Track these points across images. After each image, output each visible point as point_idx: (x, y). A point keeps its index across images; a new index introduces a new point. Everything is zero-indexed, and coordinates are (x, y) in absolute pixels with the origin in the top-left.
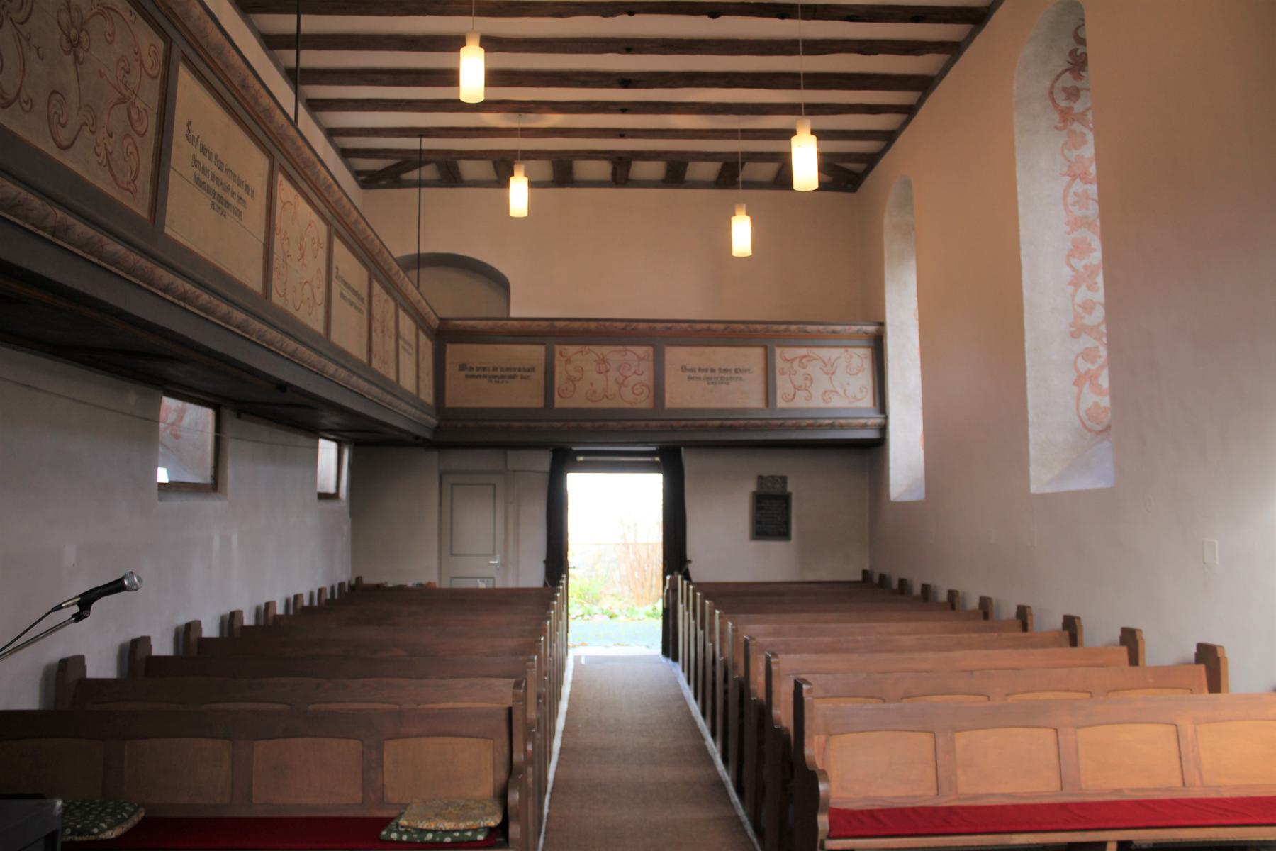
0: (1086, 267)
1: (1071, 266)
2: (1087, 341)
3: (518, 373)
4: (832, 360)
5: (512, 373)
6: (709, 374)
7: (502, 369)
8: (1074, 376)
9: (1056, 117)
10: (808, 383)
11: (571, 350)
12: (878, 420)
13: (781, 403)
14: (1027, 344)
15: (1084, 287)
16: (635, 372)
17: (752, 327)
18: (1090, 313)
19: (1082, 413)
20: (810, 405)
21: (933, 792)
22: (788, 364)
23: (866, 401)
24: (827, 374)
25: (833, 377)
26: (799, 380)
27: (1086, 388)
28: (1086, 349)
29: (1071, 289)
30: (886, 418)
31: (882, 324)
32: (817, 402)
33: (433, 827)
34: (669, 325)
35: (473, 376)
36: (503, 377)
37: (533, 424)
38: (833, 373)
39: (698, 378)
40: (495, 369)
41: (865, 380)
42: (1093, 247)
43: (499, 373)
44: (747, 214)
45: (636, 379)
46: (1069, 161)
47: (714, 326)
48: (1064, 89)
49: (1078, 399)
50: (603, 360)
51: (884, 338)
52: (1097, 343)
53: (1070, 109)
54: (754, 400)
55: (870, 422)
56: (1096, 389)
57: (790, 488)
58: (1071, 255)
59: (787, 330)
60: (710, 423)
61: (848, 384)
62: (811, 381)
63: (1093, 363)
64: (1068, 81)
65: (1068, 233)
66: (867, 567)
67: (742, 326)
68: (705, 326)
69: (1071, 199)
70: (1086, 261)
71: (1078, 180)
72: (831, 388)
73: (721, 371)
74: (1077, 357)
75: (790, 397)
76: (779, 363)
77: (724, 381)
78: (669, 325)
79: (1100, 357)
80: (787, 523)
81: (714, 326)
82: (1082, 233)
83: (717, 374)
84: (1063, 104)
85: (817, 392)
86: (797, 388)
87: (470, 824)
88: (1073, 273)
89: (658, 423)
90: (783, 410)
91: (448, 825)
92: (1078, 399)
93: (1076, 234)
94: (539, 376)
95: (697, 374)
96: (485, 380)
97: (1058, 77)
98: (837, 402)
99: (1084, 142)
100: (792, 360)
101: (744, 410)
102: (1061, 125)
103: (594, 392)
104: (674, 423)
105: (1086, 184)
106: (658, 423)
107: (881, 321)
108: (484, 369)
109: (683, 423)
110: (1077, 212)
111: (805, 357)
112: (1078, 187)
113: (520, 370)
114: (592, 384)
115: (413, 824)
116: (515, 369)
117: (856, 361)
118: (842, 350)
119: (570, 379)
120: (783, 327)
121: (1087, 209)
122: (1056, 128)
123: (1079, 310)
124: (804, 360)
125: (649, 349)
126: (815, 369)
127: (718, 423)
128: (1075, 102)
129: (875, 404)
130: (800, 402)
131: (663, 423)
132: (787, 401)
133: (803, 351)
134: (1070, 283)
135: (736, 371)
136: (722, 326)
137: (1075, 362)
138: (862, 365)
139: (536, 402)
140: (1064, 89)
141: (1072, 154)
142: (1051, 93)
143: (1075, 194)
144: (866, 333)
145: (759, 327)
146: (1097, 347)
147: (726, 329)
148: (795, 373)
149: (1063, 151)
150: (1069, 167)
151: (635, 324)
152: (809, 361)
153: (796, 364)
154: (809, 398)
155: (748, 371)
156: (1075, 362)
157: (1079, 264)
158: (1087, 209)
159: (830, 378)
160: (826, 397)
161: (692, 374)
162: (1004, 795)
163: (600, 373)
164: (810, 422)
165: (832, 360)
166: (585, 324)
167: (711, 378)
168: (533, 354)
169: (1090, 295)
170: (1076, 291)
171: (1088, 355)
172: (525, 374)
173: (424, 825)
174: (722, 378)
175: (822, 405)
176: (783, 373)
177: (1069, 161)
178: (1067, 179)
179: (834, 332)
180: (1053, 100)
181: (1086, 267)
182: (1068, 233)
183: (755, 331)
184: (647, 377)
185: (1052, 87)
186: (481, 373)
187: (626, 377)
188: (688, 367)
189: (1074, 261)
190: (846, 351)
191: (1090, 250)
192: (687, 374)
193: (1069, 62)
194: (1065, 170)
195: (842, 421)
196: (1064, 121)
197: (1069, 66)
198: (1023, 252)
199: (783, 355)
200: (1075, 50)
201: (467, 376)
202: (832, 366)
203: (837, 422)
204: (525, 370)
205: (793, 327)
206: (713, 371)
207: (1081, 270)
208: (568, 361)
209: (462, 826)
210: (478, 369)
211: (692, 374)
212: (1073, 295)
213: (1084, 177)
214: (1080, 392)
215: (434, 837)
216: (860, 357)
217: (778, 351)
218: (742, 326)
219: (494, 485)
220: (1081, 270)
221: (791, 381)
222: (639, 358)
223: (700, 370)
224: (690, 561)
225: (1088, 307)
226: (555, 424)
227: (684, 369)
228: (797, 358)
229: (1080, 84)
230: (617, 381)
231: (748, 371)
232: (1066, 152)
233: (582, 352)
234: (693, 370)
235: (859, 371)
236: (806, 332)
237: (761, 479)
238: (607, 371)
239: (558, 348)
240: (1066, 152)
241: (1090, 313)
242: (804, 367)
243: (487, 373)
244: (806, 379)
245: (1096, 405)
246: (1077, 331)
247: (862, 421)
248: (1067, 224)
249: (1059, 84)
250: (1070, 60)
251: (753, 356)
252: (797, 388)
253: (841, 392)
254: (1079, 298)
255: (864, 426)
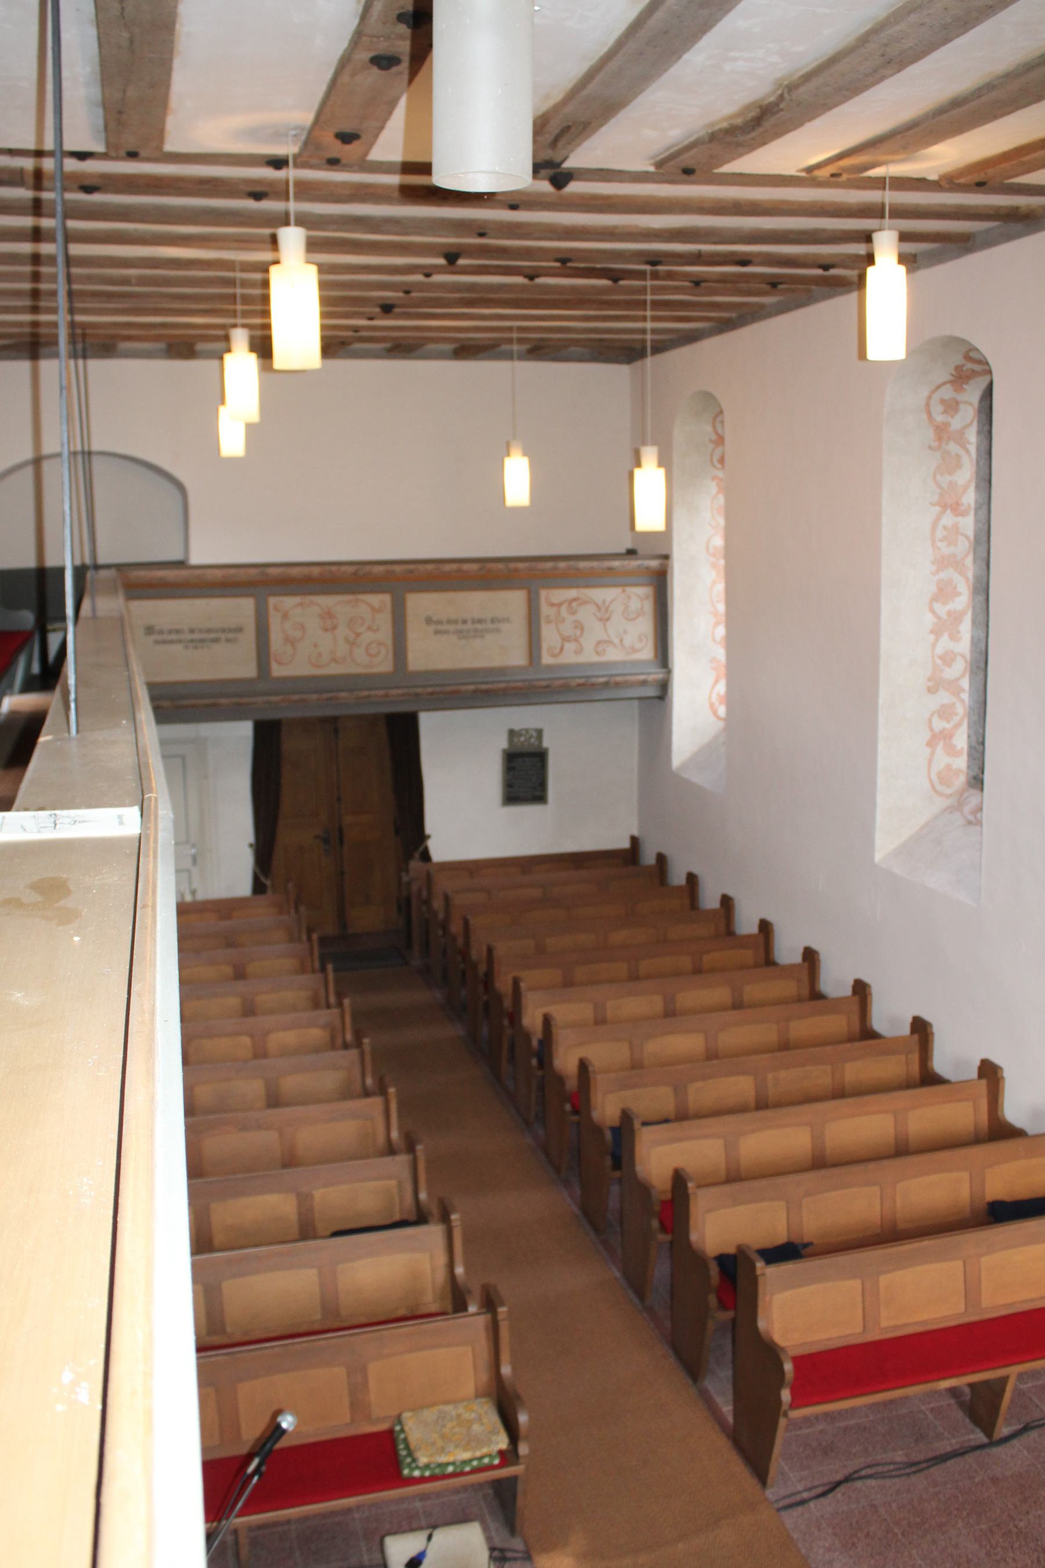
0: (949, 613)
1: (932, 611)
2: (944, 697)
3: (223, 636)
4: (607, 603)
5: (213, 636)
6: (460, 627)
7: (201, 631)
8: (928, 735)
9: (931, 433)
10: (578, 632)
11: (289, 602)
12: (658, 675)
13: (547, 659)
14: (881, 701)
15: (945, 637)
16: (369, 628)
17: (512, 565)
18: (950, 665)
19: (934, 777)
20: (581, 659)
21: (860, 1329)
22: (554, 610)
23: (647, 652)
24: (600, 620)
25: (608, 624)
26: (568, 629)
27: (940, 748)
28: (943, 706)
29: (932, 637)
30: (669, 672)
31: (666, 557)
32: (589, 656)
33: (451, 1459)
34: (411, 567)
35: (164, 642)
36: (203, 641)
37: (244, 700)
38: (608, 619)
39: (447, 632)
40: (192, 631)
41: (645, 625)
42: (945, 543)
43: (197, 636)
44: (525, 454)
45: (368, 637)
46: (941, 488)
47: (466, 567)
48: (943, 401)
49: (930, 761)
50: (328, 615)
51: (669, 577)
52: (954, 700)
53: (946, 425)
54: (517, 658)
55: (651, 678)
56: (952, 751)
57: (546, 743)
58: (935, 599)
59: (555, 568)
60: (464, 688)
61: (625, 632)
62: (582, 629)
63: (948, 721)
64: (948, 393)
65: (933, 574)
66: (636, 833)
67: (501, 566)
68: (454, 566)
69: (940, 533)
70: (950, 606)
71: (949, 511)
72: (605, 638)
73: (474, 621)
74: (932, 715)
75: (557, 651)
76: (545, 610)
77: (478, 634)
78: (411, 567)
79: (956, 714)
80: (542, 785)
81: (466, 567)
82: (950, 573)
83: (469, 626)
84: (940, 418)
85: (589, 642)
86: (565, 639)
87: (485, 1450)
88: (935, 620)
89: (400, 691)
90: (550, 667)
91: (466, 1455)
92: (930, 761)
93: (942, 575)
94: (249, 637)
95: (446, 627)
96: (179, 647)
97: (938, 387)
98: (613, 655)
99: (959, 466)
100: (559, 605)
101: (502, 671)
102: (935, 444)
103: (320, 655)
104: (419, 690)
105: (957, 515)
106: (400, 691)
107: (664, 552)
108: (178, 632)
109: (430, 690)
110: (946, 550)
111: (575, 600)
112: (948, 519)
113: (223, 630)
114: (315, 645)
115: (433, 1460)
116: (217, 631)
117: (635, 604)
118: (619, 590)
119: (289, 640)
120: (549, 565)
121: (956, 546)
122: (930, 447)
123: (939, 662)
124: (574, 605)
125: (387, 598)
126: (585, 614)
127: (472, 687)
128: (952, 417)
129: (656, 656)
130: (569, 657)
131: (405, 690)
132: (554, 656)
133: (573, 593)
134: (932, 632)
135: (493, 621)
136: (475, 567)
137: (930, 721)
138: (642, 607)
139: (248, 670)
140: (943, 401)
141: (945, 480)
142: (928, 405)
143: (945, 528)
144: (648, 568)
145: (521, 565)
146: (954, 704)
147: (481, 569)
148: (563, 621)
149: (935, 476)
150: (941, 495)
151: (368, 568)
152: (580, 605)
153: (564, 609)
154: (579, 651)
155: (507, 620)
156: (930, 721)
157: (942, 610)
158: (956, 546)
159: (605, 626)
160: (600, 649)
161: (440, 627)
162: (916, 1323)
163: (326, 630)
164: (581, 681)
165: (607, 603)
166: (305, 571)
167: (461, 631)
168: (243, 608)
169: (951, 645)
170: (937, 640)
171: (944, 712)
172: (231, 636)
173: (443, 1459)
174: (476, 631)
175: (595, 659)
176: (549, 622)
177: (941, 488)
178: (938, 509)
179: (610, 569)
180: (929, 413)
181: (949, 613)
182: (933, 574)
183: (516, 570)
184: (385, 633)
185: (929, 397)
186: (174, 637)
187: (358, 635)
188: (435, 619)
189: (937, 606)
190: (624, 591)
191: (957, 594)
192: (432, 628)
193: (952, 375)
194: (936, 498)
195: (619, 679)
196: (939, 439)
197: (951, 378)
198: (883, 596)
199: (552, 597)
200: (963, 366)
201: (157, 642)
202: (607, 610)
203: (613, 680)
204: (230, 630)
205: (562, 565)
206: (465, 622)
207: (944, 616)
208: (285, 616)
209: (478, 1454)
210: (170, 632)
211: (440, 627)
212: (934, 645)
213: (956, 509)
214: (933, 754)
215: (455, 1468)
216: (640, 597)
217: (543, 593)
218: (501, 566)
219: (183, 758)
220: (944, 616)
221: (558, 630)
222: (373, 609)
223: (450, 622)
224: (429, 837)
225: (948, 659)
226: (273, 698)
227: (429, 621)
228: (565, 601)
229: (960, 397)
230: (347, 640)
231: (507, 620)
232: (938, 477)
233: (301, 604)
234: (440, 622)
235: (638, 616)
236: (577, 569)
237: (512, 733)
238: (334, 628)
239: (272, 601)
240: (938, 477)
241: (950, 665)
242: (573, 612)
243: (182, 637)
244: (576, 627)
245: (948, 767)
246: (934, 686)
247: (642, 677)
248: (933, 563)
249: (937, 396)
250: (953, 372)
251: (513, 601)
252: (565, 639)
253: (616, 641)
254: (939, 650)
255: (644, 683)
